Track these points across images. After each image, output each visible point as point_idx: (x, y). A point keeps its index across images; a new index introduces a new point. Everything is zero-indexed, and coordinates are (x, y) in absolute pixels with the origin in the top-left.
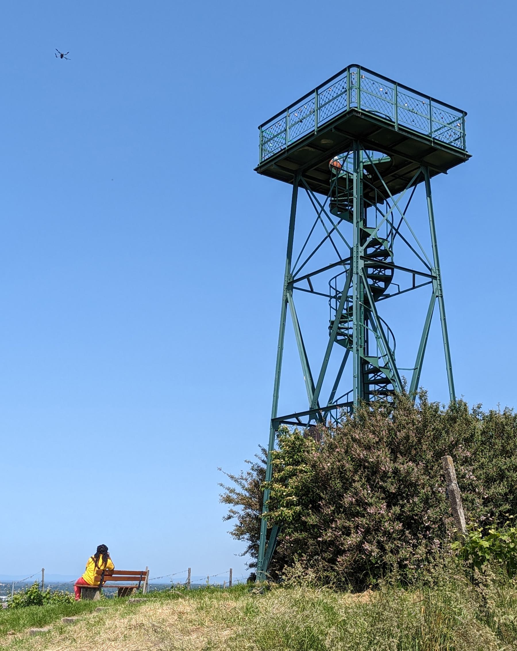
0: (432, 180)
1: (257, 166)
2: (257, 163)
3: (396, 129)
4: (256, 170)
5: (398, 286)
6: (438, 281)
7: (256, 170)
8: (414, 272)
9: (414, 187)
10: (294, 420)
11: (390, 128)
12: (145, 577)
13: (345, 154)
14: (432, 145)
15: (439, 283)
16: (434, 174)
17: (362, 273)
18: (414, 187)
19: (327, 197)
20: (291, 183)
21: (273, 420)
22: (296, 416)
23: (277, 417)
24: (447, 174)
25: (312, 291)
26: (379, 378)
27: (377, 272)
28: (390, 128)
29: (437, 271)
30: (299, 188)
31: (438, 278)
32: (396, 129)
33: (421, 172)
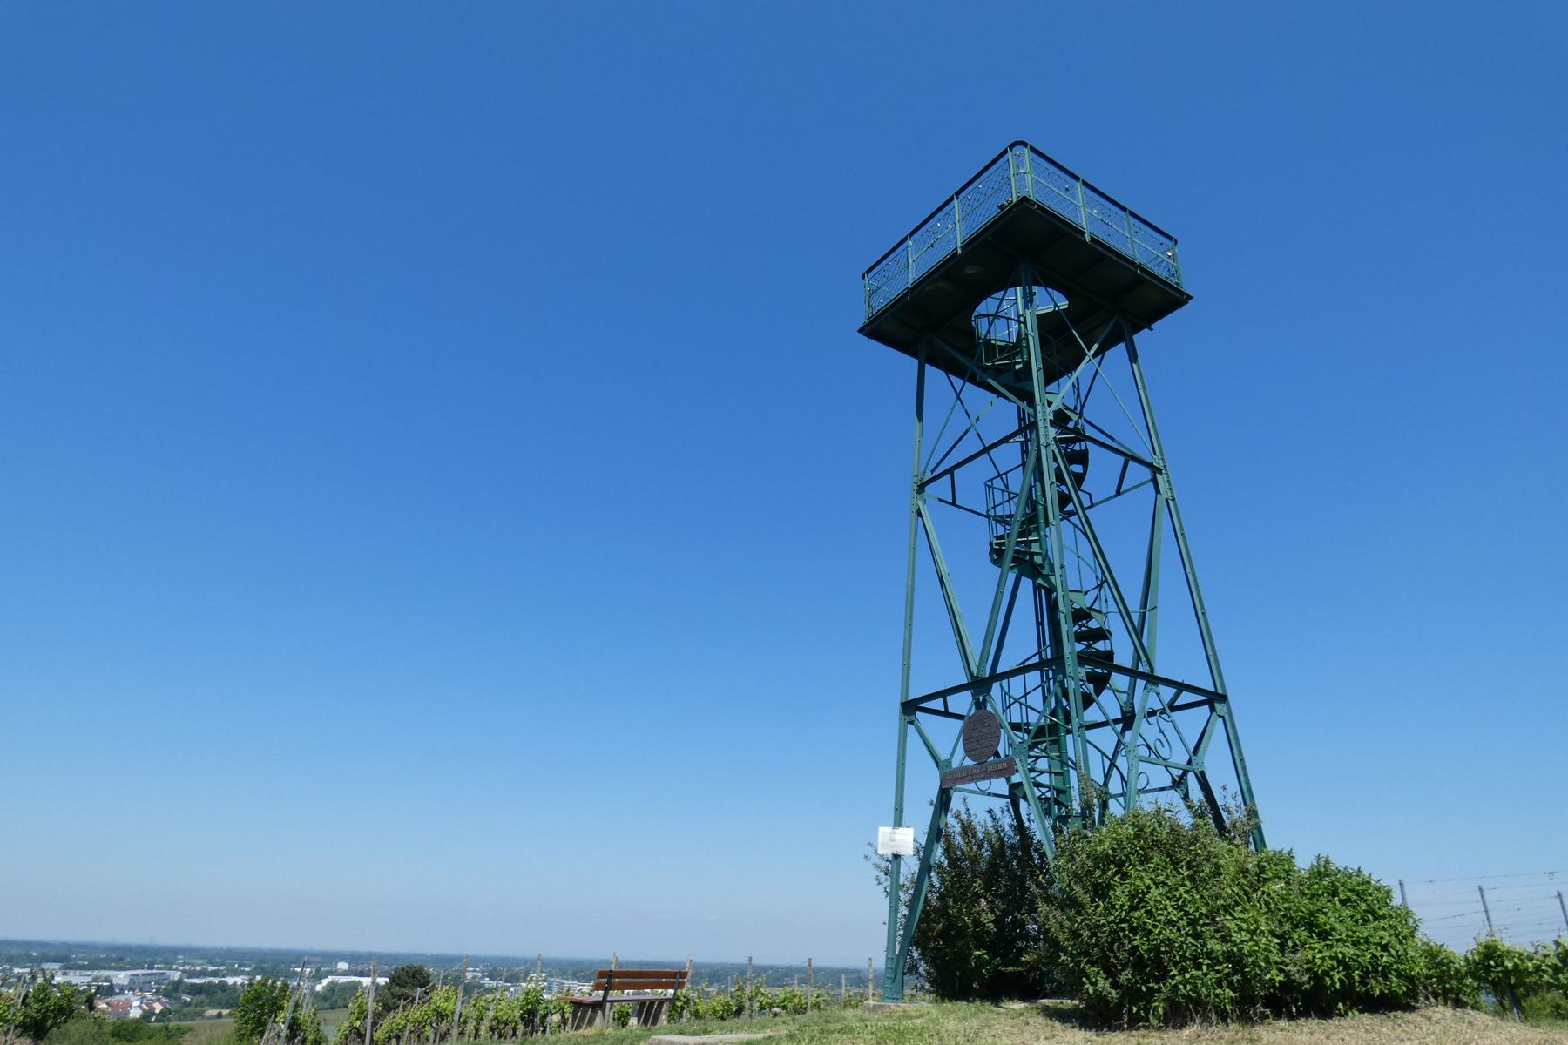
0: (1137, 338)
1: (862, 325)
2: (862, 322)
3: (1088, 239)
4: (860, 331)
5: (1090, 495)
6: (1164, 475)
7: (860, 331)
8: (1129, 457)
9: (1100, 357)
10: (937, 704)
11: (1079, 236)
12: (1045, 736)
13: (1000, 294)
14: (1139, 272)
15: (1166, 479)
16: (1137, 329)
17: (1055, 446)
18: (1100, 357)
19: (963, 381)
20: (914, 355)
21: (903, 704)
22: (944, 694)
23: (910, 699)
24: (1152, 330)
25: (954, 504)
26: (1084, 629)
27: (1071, 447)
28: (1079, 236)
29: (1161, 462)
30: (927, 365)
31: (1163, 472)
32: (1088, 239)
33: (1117, 321)
